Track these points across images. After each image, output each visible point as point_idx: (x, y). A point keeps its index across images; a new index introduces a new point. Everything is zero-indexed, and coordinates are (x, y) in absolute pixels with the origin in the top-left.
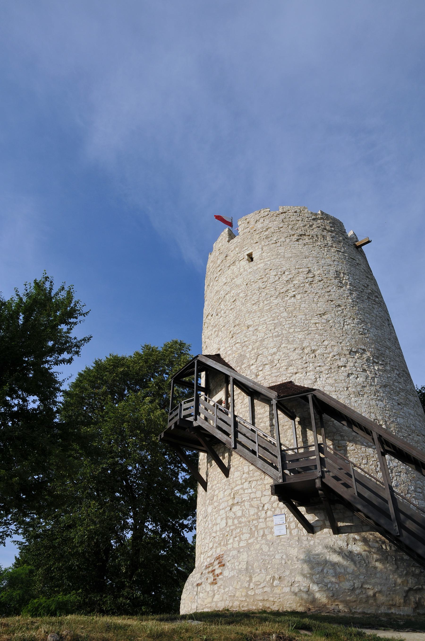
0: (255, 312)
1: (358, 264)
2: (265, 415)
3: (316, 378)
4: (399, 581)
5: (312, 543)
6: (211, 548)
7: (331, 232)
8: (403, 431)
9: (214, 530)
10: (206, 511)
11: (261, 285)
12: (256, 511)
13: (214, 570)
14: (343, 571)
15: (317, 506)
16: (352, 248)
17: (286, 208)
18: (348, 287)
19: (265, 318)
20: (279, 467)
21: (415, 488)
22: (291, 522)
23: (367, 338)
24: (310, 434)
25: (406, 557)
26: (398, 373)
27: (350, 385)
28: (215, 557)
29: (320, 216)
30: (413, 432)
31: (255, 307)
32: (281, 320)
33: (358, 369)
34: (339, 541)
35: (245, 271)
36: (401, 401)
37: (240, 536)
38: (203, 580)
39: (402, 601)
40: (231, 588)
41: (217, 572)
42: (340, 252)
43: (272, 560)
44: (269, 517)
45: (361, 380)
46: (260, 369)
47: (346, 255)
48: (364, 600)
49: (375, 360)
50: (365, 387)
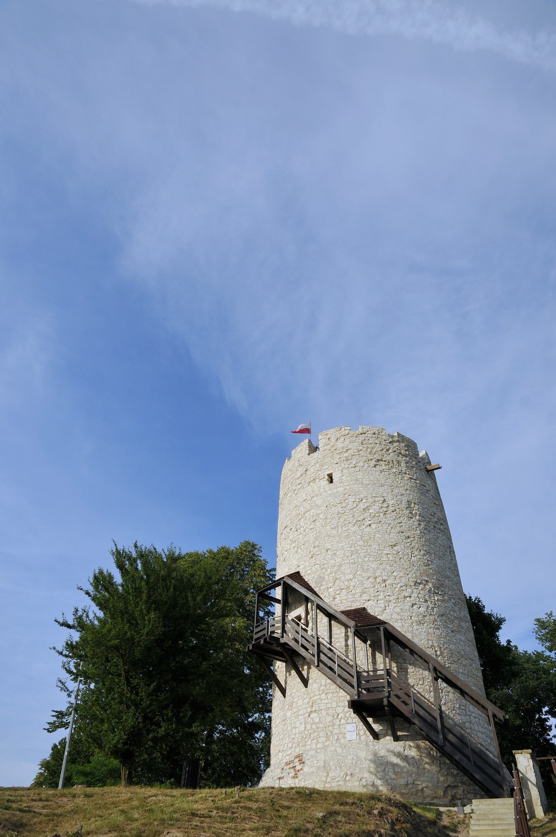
0: (334, 536)
1: (427, 490)
2: (341, 636)
3: (385, 607)
4: (442, 779)
5: (377, 747)
6: (290, 748)
7: (406, 456)
8: (454, 656)
9: (294, 732)
10: (285, 715)
11: (340, 509)
12: (332, 719)
13: (295, 767)
14: (400, 770)
15: (382, 718)
16: (424, 473)
17: (366, 428)
18: (417, 517)
19: (343, 544)
20: (355, 685)
21: (460, 706)
22: (361, 730)
23: (430, 569)
24: (379, 657)
25: (448, 761)
26: (454, 602)
27: (414, 614)
28: (295, 755)
29: (396, 439)
30: (462, 656)
31: (334, 532)
32: (357, 548)
33: (421, 599)
34: (398, 746)
35: (325, 491)
36: (455, 628)
37: (317, 739)
38: (284, 774)
39: (442, 794)
40: (311, 781)
41: (298, 768)
42: (412, 479)
43: (345, 760)
44: (343, 725)
45: (422, 610)
46: (338, 593)
47: (418, 482)
48: (414, 793)
49: (435, 590)
50: (425, 616)
